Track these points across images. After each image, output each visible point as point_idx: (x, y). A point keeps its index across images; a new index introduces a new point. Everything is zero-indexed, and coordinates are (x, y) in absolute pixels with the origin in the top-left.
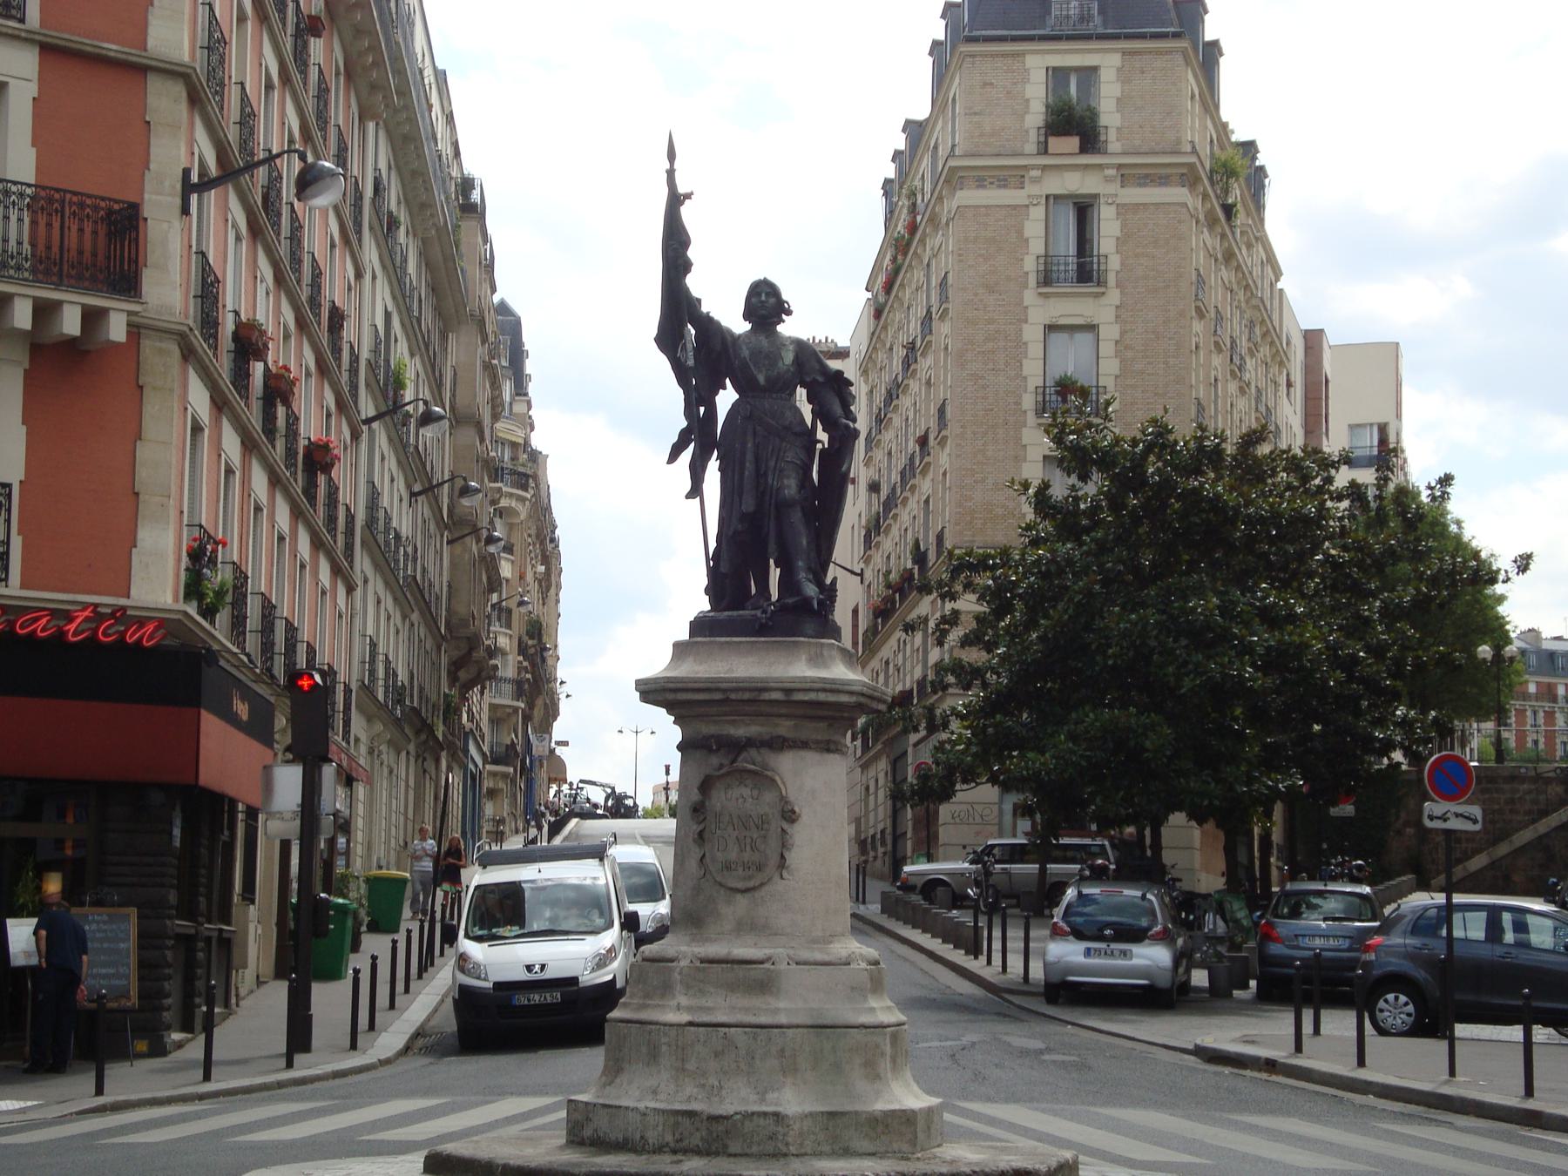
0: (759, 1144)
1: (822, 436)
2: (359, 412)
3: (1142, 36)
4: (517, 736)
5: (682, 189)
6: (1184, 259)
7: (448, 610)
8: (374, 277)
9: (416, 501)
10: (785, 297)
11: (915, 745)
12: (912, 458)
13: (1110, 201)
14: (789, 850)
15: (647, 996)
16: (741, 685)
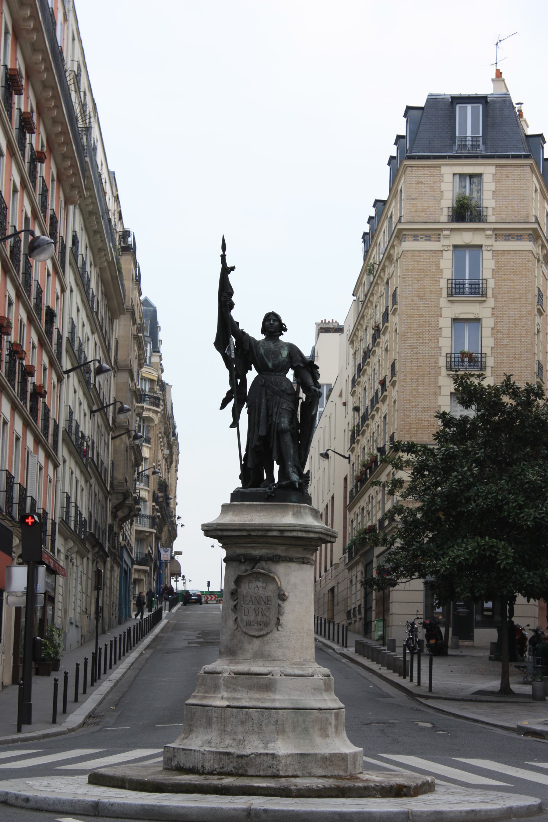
0: (264, 770)
1: (302, 395)
2: (62, 367)
3: (507, 157)
4: (152, 549)
5: (229, 265)
6: (531, 282)
7: (112, 477)
8: (72, 291)
9: (94, 415)
10: (283, 322)
11: (378, 557)
12: (377, 393)
13: (489, 249)
14: (282, 615)
15: (206, 692)
16: (257, 527)
